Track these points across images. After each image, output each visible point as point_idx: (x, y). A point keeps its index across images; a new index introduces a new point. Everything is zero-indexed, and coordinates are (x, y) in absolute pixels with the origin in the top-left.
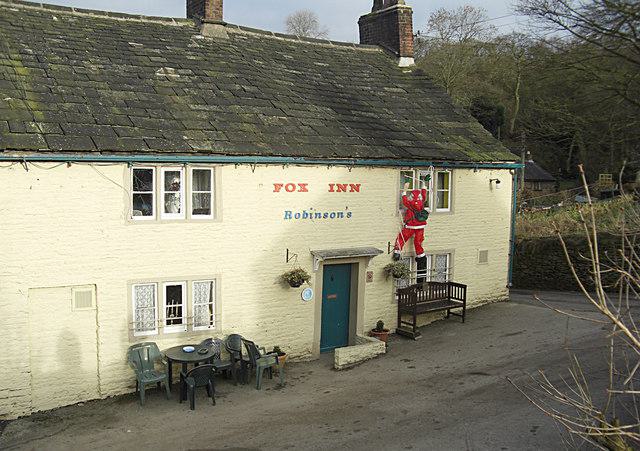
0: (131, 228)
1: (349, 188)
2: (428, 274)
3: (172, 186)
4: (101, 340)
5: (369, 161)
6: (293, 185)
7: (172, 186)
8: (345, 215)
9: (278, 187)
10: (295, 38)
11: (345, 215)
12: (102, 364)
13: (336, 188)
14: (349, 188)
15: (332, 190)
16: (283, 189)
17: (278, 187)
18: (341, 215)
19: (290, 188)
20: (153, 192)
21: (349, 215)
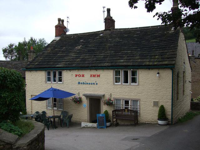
0: (46, 84)
1: (96, 76)
2: (129, 106)
3: (55, 76)
4: (188, 51)
5: (98, 62)
6: (79, 76)
7: (55, 76)
8: (95, 84)
9: (76, 76)
10: (153, 120)
11: (95, 84)
12: (33, 111)
13: (92, 76)
14: (96, 76)
15: (91, 76)
16: (78, 76)
17: (76, 76)
18: (94, 84)
19: (79, 76)
20: (131, 77)
21: (97, 84)
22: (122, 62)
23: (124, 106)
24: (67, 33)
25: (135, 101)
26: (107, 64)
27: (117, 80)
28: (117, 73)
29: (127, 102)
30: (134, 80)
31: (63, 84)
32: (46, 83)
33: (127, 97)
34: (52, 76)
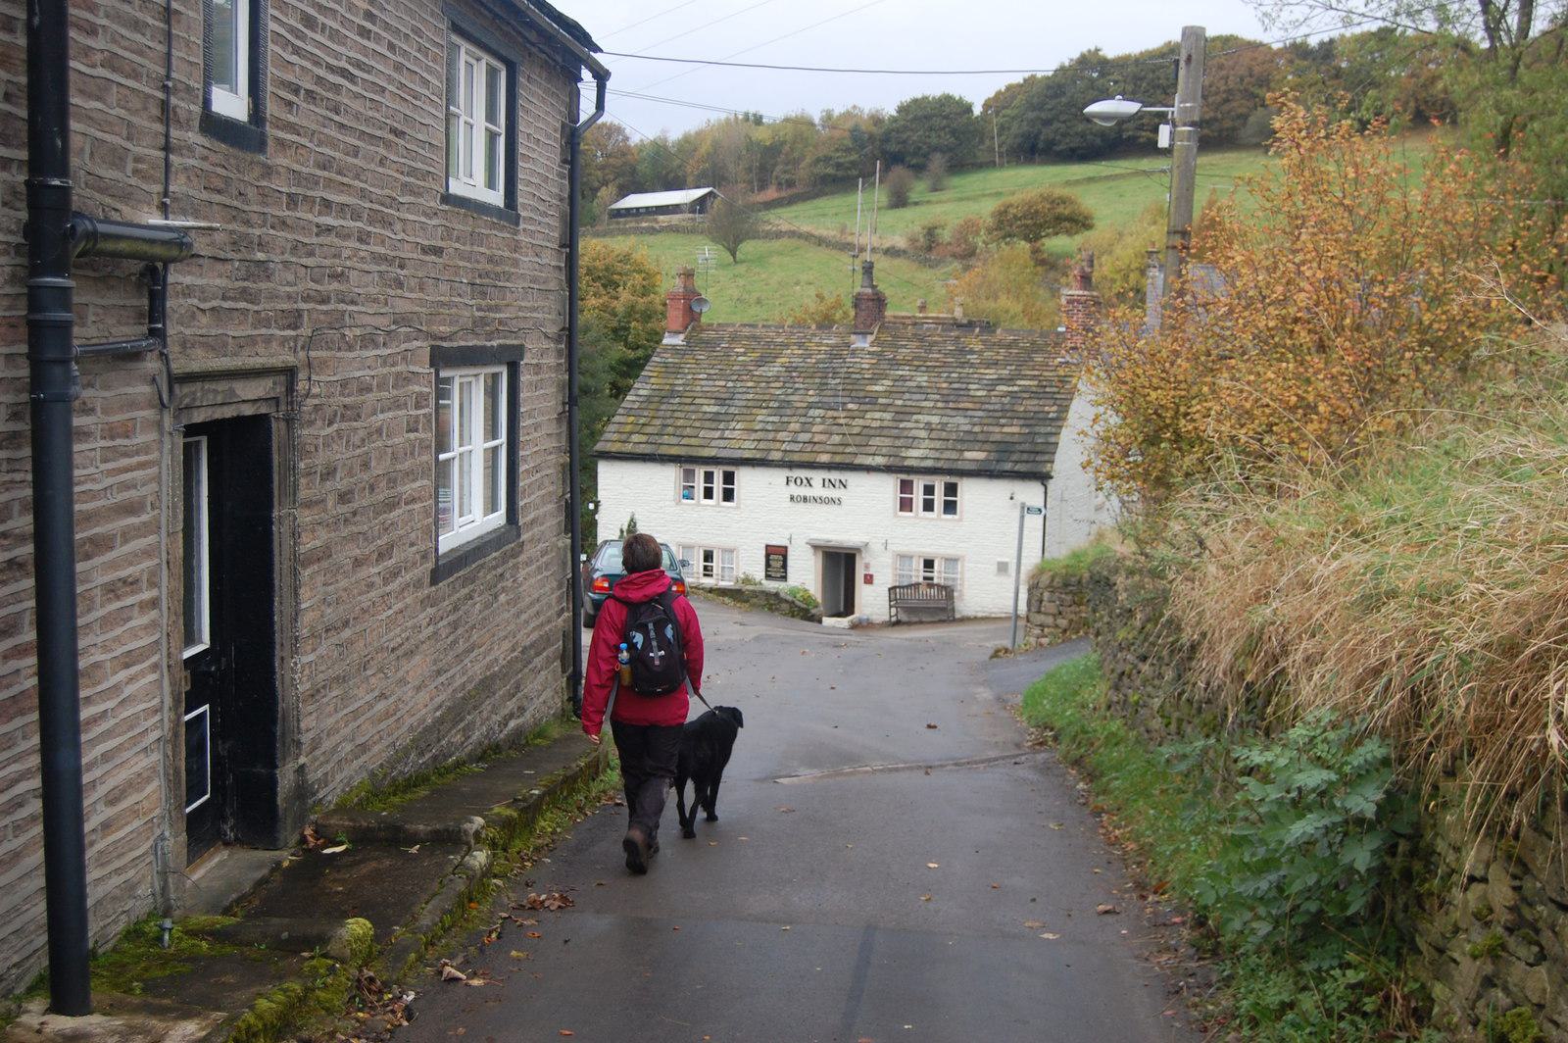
22: (914, 455)
23: (922, 574)
24: (977, 111)
25: (952, 561)
26: (879, 460)
27: (906, 505)
28: (689, 475)
29: (929, 564)
30: (950, 507)
31: (738, 507)
32: (896, 515)
33: (929, 551)
34: (700, 484)
